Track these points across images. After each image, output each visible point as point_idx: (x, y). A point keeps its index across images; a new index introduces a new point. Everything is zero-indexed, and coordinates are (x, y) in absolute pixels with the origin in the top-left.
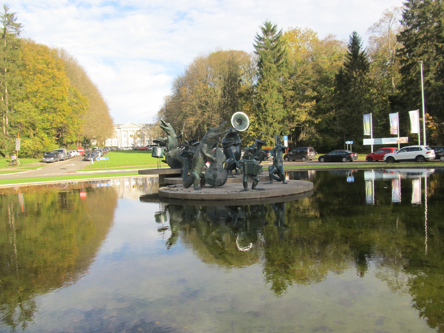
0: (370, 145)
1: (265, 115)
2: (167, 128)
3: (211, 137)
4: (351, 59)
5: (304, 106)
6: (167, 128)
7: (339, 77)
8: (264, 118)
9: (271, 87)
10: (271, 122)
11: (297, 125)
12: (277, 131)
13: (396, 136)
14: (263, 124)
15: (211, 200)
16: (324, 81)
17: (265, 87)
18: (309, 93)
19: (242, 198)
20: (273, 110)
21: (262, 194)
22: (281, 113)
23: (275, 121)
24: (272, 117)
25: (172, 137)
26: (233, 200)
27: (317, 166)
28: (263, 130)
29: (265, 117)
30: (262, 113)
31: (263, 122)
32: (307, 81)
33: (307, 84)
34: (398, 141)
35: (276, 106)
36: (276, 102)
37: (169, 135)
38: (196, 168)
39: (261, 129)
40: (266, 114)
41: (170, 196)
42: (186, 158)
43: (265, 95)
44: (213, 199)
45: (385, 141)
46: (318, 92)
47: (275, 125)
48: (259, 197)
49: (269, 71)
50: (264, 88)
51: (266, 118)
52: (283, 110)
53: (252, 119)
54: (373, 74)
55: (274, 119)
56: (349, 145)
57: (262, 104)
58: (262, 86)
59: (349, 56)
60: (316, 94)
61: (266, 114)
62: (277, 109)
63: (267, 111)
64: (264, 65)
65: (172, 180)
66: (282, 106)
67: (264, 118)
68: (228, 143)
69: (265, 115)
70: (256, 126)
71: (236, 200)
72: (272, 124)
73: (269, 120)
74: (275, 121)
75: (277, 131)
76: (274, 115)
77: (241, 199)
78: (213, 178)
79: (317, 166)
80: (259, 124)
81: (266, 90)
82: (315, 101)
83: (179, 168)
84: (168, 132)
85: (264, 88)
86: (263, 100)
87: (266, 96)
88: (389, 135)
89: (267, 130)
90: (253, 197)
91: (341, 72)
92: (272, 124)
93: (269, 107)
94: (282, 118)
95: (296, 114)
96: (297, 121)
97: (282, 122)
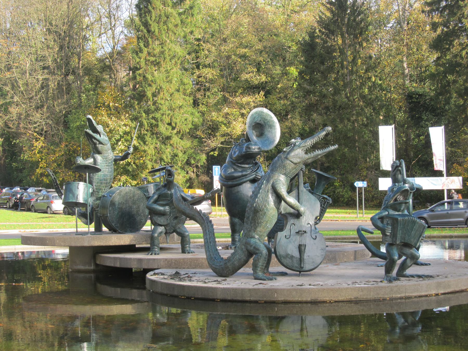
0: (443, 191)
1: (153, 118)
2: (97, 136)
3: (299, 160)
4: (332, 12)
5: (237, 103)
6: (97, 136)
7: (309, 47)
8: (151, 126)
9: (168, 58)
10: (168, 134)
11: (222, 143)
12: (180, 154)
13: (439, 174)
14: (148, 138)
15: (266, 302)
16: (277, 54)
17: (154, 56)
18: (251, 76)
19: (403, 295)
20: (171, 109)
21: (439, 285)
22: (187, 117)
23: (175, 131)
24: (170, 124)
25: (105, 158)
26: (384, 300)
27: (340, 233)
28: (149, 152)
29: (153, 121)
30: (147, 112)
31: (149, 134)
32: (243, 51)
33: (243, 57)
34: (444, 185)
35: (179, 100)
36: (178, 91)
37: (99, 153)
38: (259, 229)
39: (146, 148)
40: (158, 115)
41: (220, 296)
42: (167, 208)
43: (156, 73)
44: (341, 299)
45: (426, 183)
46: (267, 74)
47: (175, 139)
48: (433, 292)
49: (165, 23)
50: (152, 59)
51: (157, 126)
52: (191, 109)
53: (125, 125)
54: (378, 46)
55: (173, 128)
56: (360, 188)
57: (149, 94)
58: (149, 53)
59: (328, 6)
60: (263, 78)
61: (158, 115)
62: (180, 107)
63: (157, 109)
64: (153, 8)
65: (140, 260)
66: (190, 100)
67: (151, 126)
68: (239, 177)
69: (153, 118)
70: (135, 142)
71: (392, 299)
72: (169, 138)
73: (163, 129)
74: (175, 131)
75: (180, 154)
76: (174, 120)
77: (401, 298)
78: (296, 254)
79: (332, 233)
80: (141, 138)
81: (157, 64)
82: (262, 93)
83: (131, 232)
84: (99, 146)
85: (152, 59)
86: (150, 85)
87: (157, 75)
88: (429, 170)
89: (158, 151)
90: (423, 294)
91: (312, 35)
92: (169, 138)
93: (163, 102)
94: (190, 126)
95: (221, 119)
96: (223, 135)
97: (192, 134)
